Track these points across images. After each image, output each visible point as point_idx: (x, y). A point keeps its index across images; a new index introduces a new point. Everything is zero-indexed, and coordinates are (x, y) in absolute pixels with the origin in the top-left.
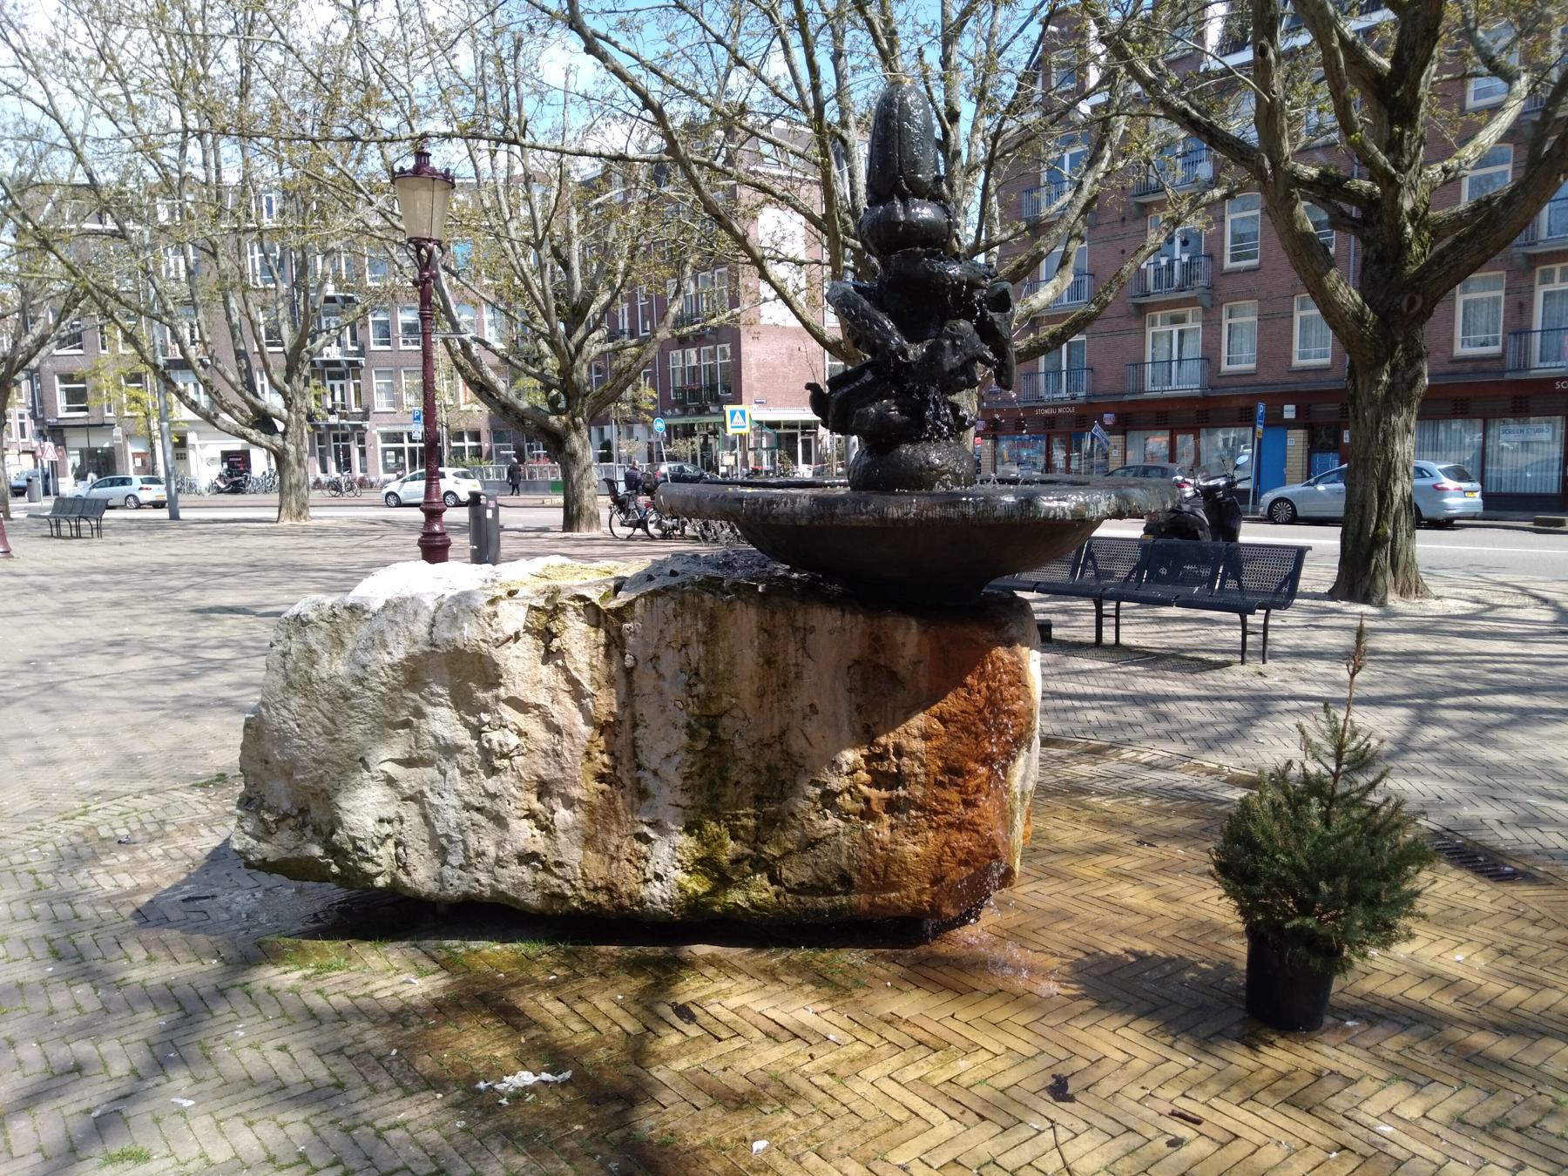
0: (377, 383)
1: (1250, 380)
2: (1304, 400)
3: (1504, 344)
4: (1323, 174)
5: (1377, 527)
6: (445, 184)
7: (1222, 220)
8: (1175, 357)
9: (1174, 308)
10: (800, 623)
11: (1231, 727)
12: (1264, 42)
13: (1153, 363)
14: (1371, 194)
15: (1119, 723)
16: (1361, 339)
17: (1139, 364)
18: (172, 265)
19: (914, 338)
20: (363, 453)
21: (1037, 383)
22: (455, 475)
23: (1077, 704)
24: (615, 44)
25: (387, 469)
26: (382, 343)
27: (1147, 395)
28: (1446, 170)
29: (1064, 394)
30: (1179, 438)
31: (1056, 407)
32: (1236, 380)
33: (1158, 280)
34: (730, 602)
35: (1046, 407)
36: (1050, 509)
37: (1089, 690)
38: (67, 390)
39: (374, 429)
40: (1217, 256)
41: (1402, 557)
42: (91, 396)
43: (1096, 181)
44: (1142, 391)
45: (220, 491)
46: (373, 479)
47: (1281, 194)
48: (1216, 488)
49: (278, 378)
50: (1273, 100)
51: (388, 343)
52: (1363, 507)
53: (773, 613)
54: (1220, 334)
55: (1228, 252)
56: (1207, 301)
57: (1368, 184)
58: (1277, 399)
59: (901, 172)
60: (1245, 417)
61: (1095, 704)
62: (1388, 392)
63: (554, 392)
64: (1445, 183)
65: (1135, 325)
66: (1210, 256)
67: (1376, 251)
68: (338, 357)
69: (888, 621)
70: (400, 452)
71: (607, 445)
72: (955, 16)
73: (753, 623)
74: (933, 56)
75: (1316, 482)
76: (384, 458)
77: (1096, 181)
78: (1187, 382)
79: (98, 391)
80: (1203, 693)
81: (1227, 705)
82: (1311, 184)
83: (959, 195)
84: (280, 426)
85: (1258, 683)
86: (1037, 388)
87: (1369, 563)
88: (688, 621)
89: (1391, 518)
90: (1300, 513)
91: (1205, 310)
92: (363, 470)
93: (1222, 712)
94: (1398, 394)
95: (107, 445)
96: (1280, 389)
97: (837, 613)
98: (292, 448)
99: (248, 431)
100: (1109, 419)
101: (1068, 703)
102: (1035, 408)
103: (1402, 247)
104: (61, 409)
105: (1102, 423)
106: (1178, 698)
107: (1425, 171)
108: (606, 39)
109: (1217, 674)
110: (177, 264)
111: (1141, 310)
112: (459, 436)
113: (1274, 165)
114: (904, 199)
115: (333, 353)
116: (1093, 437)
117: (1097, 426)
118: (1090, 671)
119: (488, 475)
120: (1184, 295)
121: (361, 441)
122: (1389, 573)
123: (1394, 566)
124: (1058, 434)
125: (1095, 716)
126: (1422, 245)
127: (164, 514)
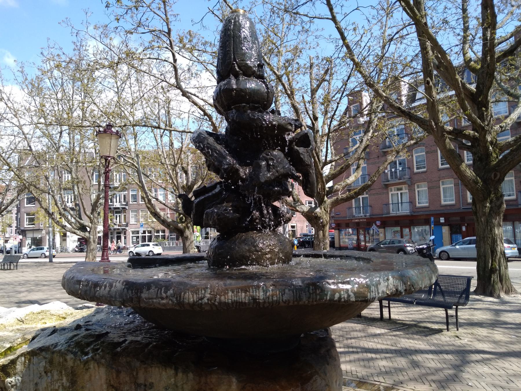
0: (131, 214)
1: (427, 209)
2: (446, 216)
3: (517, 195)
4: (454, 129)
5: (492, 265)
6: (117, 137)
7: (412, 156)
8: (400, 202)
9: (398, 185)
10: (141, 380)
11: (451, 372)
12: (428, 79)
13: (392, 204)
14: (474, 136)
15: (395, 369)
16: (477, 189)
17: (387, 204)
18: (66, 177)
19: (243, 164)
20: (125, 238)
21: (352, 211)
22: (153, 245)
23: (373, 356)
24: (198, 97)
25: (133, 243)
26: (134, 201)
27: (391, 215)
28: (501, 127)
29: (362, 214)
30: (404, 229)
31: (359, 219)
32: (422, 210)
33: (391, 176)
34: (86, 362)
35: (356, 219)
36: (334, 291)
37: (379, 346)
38: (29, 218)
39: (129, 230)
40: (411, 168)
41: (504, 277)
42: (36, 220)
43: (368, 139)
44: (389, 213)
45: (76, 251)
46: (128, 247)
47: (440, 135)
48: (423, 249)
49: (88, 213)
50: (433, 100)
51: (136, 201)
52: (485, 256)
53: (118, 372)
54: (415, 193)
55: (415, 167)
56: (409, 183)
57: (472, 132)
58: (438, 216)
59: (235, 60)
60: (427, 222)
61: (383, 355)
62: (490, 211)
63: (182, 216)
64: (502, 131)
65: (385, 191)
66: (409, 168)
67: (478, 157)
68: (119, 206)
69: (214, 378)
70: (138, 237)
71: (207, 233)
72: (315, 86)
73: (103, 381)
74: (307, 98)
75: (456, 245)
76: (132, 239)
77: (368, 139)
78: (405, 210)
79: (38, 218)
80: (433, 348)
81: (445, 356)
82: (450, 133)
83: (319, 145)
84: (88, 229)
85: (458, 342)
86: (352, 213)
87: (490, 279)
88: (56, 377)
89: (497, 261)
90: (451, 256)
91: (409, 186)
92: (125, 244)
93: (445, 361)
94: (495, 210)
95: (40, 236)
96: (438, 212)
97: (171, 372)
98: (92, 237)
99: (76, 231)
100: (378, 223)
101: (370, 355)
102: (352, 219)
103: (488, 155)
104: (26, 225)
105: (376, 225)
106: (422, 352)
107: (493, 127)
108: (195, 95)
109: (437, 336)
110: (68, 176)
111: (387, 186)
112: (158, 232)
113: (436, 124)
114: (237, 76)
115: (117, 205)
116: (373, 230)
117: (374, 226)
118: (379, 335)
119: (166, 245)
120: (401, 181)
121: (125, 234)
122: (499, 284)
123: (501, 281)
124: (361, 228)
125: (383, 364)
126: (496, 154)
127: (47, 260)
